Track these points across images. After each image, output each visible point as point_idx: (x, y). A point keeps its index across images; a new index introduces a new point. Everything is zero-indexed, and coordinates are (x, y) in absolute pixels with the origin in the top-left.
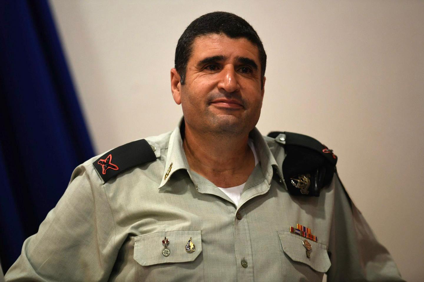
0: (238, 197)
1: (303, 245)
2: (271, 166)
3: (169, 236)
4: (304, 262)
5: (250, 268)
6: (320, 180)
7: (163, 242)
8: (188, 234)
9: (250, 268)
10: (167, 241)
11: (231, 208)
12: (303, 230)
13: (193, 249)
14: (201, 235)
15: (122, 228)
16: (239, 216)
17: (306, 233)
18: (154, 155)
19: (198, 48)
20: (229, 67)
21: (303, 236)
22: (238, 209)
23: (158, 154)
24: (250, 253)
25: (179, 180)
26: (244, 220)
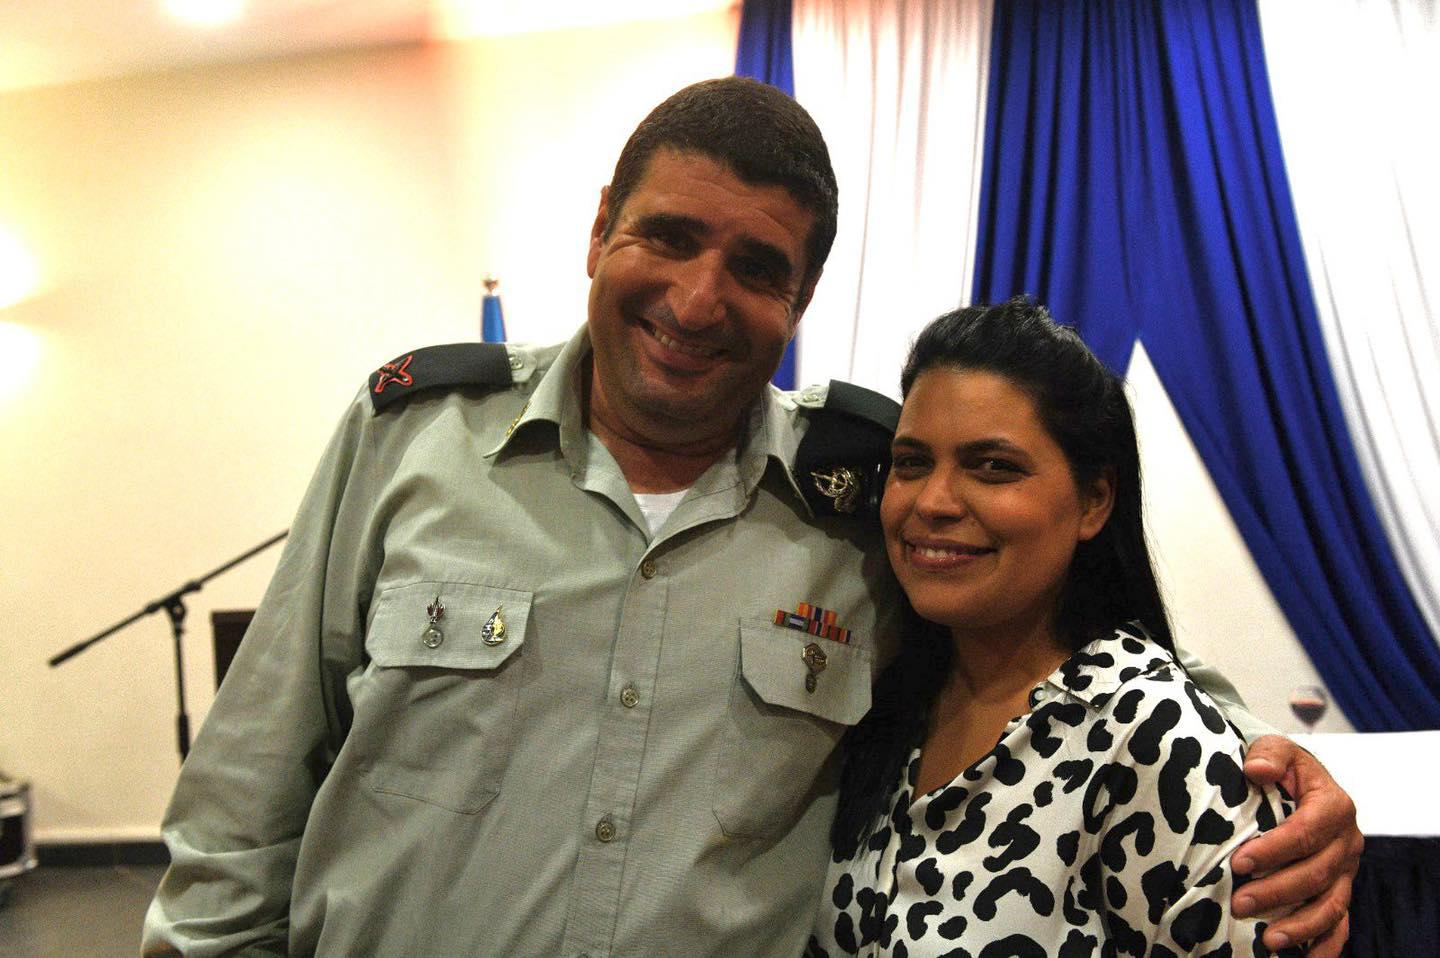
0: (660, 511)
1: (804, 659)
2: (766, 459)
3: (450, 594)
4: (803, 708)
5: (641, 709)
6: (931, 554)
7: (430, 610)
8: (499, 596)
9: (641, 709)
10: (440, 611)
11: (637, 542)
12: (813, 618)
13: (500, 635)
14: (529, 604)
15: (172, 853)
16: (649, 567)
17: (820, 625)
18: (511, 377)
19: (1311, 834)
20: (710, 258)
21: (807, 631)
22: (652, 546)
23: (521, 375)
24: (652, 670)
25: (533, 440)
26: (659, 582)
